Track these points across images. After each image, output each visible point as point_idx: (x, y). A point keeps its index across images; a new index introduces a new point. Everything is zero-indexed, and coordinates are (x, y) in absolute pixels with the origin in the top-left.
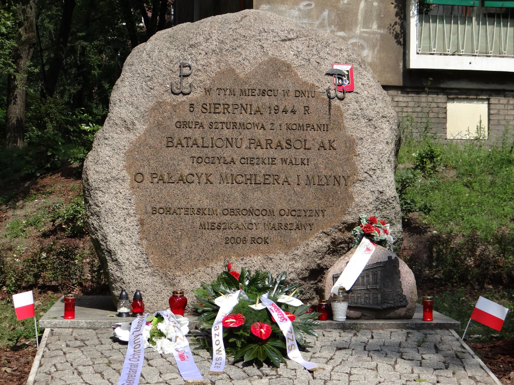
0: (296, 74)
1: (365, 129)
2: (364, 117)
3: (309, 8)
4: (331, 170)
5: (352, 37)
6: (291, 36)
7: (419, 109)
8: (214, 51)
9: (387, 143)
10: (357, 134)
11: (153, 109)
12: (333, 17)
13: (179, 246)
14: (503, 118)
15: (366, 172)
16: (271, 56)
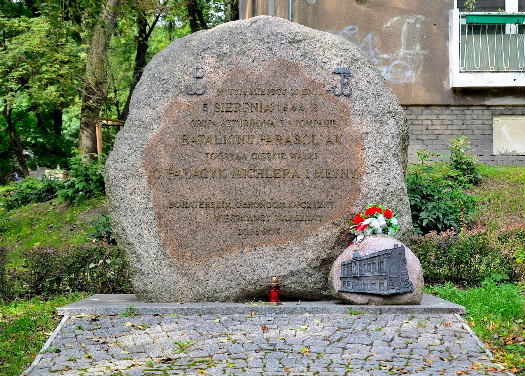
3: (353, 32)
5: (396, 59)
7: (464, 127)
15: (373, 165)
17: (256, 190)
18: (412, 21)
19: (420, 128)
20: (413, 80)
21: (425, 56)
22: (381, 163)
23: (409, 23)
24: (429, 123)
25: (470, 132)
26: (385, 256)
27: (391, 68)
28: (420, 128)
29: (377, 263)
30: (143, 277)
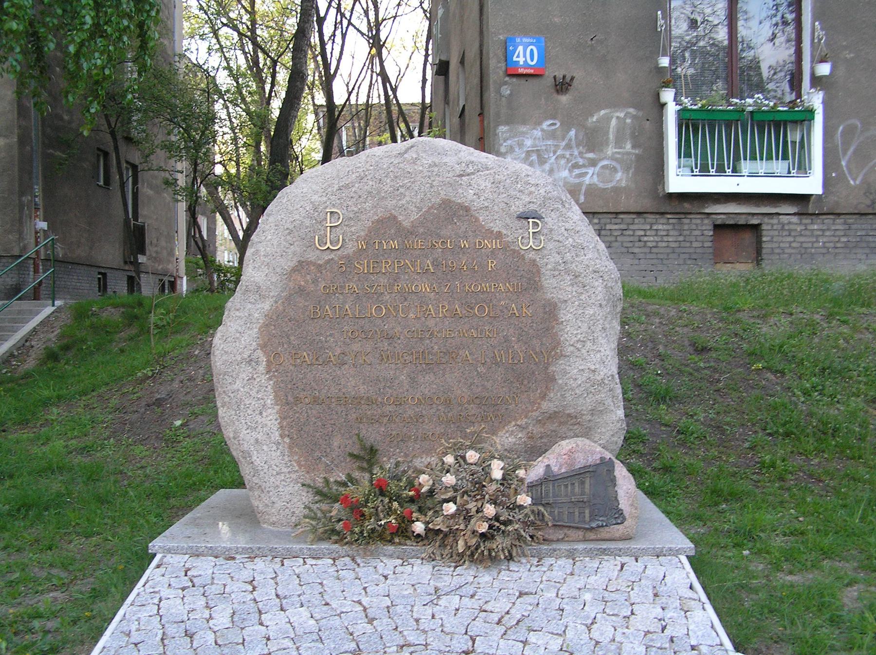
0: (477, 220)
1: (569, 289)
2: (568, 272)
3: (553, 128)
4: (526, 343)
5: (603, 159)
6: (470, 169)
7: (681, 238)
8: (370, 193)
9: (601, 305)
10: (563, 296)
11: (294, 270)
12: (581, 137)
13: (330, 445)
14: (777, 245)
15: (572, 345)
16: (444, 197)
17: (413, 380)
18: (622, 115)
19: (631, 239)
20: (623, 184)
21: (636, 155)
22: (584, 341)
23: (618, 117)
24: (642, 233)
25: (688, 244)
26: (588, 475)
27: (597, 168)
28: (631, 239)
29: (576, 484)
30: (262, 495)
